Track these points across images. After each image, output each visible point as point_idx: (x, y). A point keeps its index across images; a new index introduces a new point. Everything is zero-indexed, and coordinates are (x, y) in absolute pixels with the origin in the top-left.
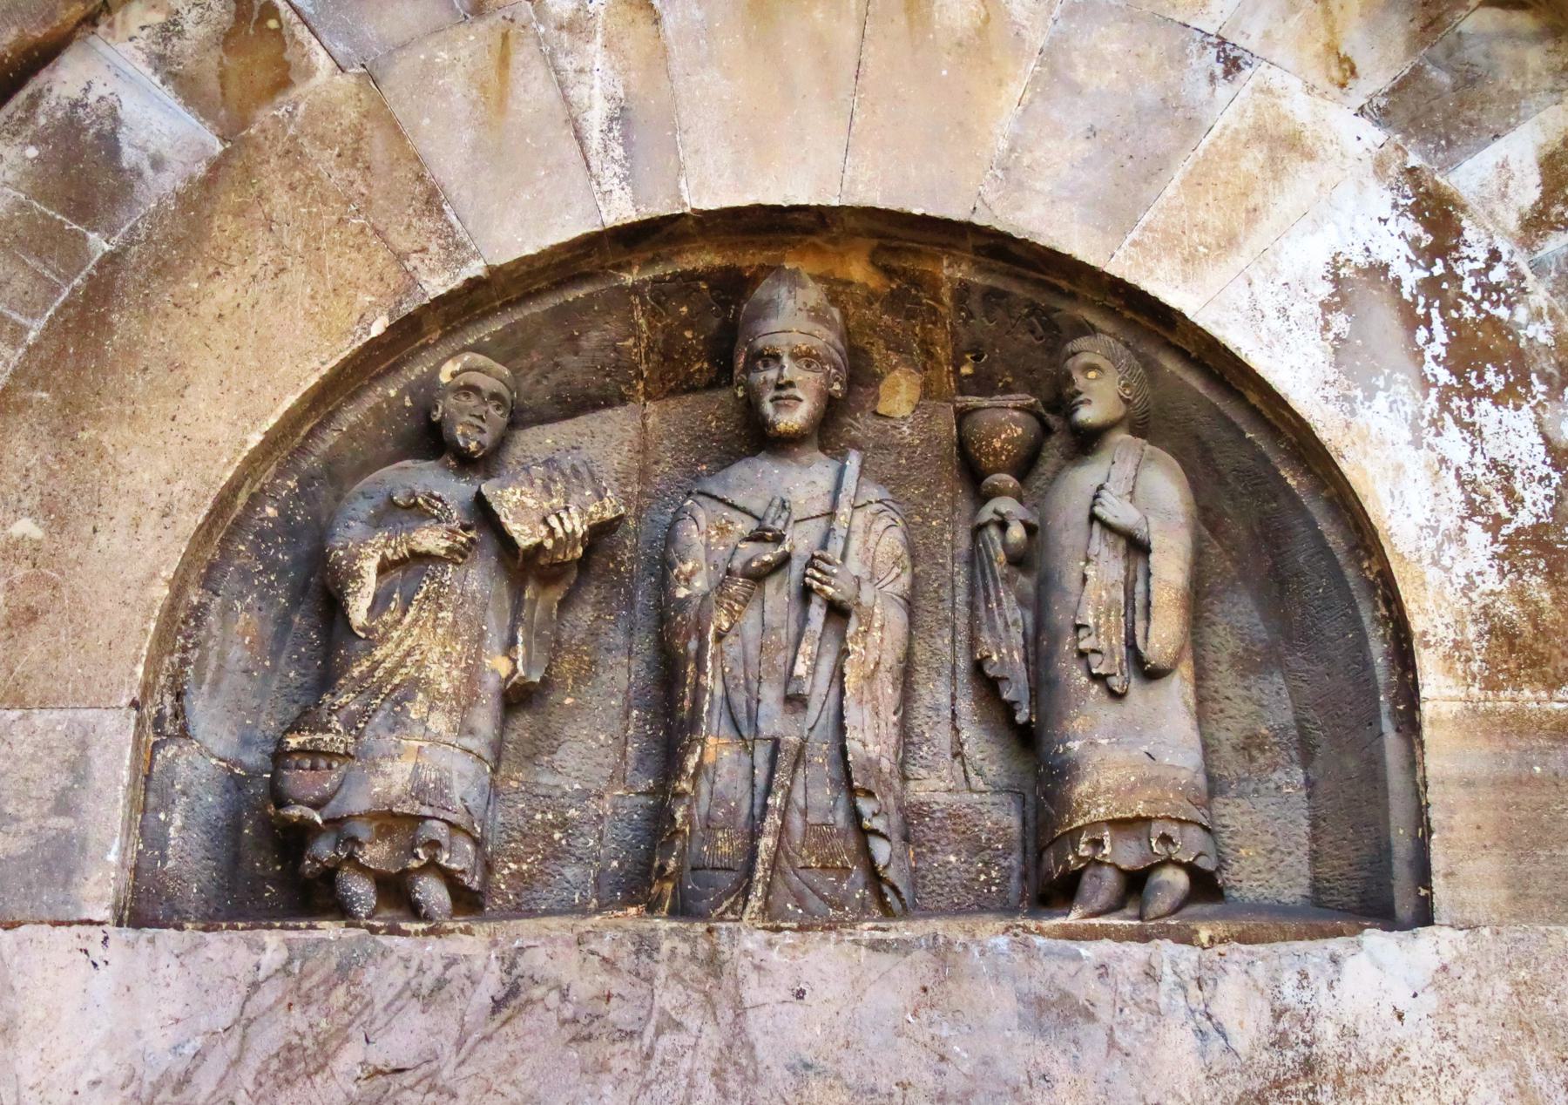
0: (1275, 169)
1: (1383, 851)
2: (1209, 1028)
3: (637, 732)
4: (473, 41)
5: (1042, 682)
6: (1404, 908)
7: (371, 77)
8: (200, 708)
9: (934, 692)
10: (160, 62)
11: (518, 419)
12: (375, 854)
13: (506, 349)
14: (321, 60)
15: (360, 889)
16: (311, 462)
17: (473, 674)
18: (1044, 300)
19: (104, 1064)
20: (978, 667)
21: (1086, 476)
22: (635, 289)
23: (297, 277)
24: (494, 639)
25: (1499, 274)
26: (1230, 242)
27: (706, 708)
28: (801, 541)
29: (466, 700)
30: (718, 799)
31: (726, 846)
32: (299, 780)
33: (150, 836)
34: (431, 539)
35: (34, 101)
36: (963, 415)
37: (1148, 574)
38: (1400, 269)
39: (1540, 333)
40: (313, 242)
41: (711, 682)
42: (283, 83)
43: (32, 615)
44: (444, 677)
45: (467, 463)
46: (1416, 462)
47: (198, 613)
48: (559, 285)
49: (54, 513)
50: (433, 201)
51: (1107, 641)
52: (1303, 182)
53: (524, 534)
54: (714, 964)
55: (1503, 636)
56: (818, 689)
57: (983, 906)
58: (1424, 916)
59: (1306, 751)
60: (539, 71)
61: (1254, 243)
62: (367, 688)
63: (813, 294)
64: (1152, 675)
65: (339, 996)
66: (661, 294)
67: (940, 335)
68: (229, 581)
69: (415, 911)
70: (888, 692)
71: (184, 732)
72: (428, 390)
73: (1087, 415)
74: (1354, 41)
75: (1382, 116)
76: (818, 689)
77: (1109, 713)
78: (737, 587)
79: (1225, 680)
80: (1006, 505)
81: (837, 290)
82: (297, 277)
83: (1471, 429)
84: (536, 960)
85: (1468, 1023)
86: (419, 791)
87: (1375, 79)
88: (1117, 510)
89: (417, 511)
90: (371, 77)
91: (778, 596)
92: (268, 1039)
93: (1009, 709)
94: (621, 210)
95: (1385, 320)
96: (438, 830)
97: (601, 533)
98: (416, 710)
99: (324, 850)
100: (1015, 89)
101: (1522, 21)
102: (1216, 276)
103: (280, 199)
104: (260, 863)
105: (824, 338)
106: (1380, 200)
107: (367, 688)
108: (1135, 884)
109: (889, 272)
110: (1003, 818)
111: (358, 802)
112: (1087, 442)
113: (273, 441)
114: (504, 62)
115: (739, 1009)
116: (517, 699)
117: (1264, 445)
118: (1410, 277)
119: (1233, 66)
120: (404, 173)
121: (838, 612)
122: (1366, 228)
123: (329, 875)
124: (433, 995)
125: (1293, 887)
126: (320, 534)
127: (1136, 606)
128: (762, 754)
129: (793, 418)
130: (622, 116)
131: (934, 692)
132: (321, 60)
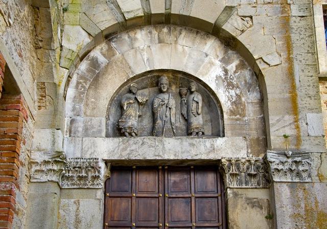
1: (219, 131)
2: (205, 146)
3: (150, 120)
6: (221, 136)
7: (123, 55)
8: (110, 117)
10: (101, 53)
14: (117, 53)
15: (127, 134)
16: (119, 94)
17: (136, 114)
18: (189, 79)
19: (106, 150)
20: (182, 114)
21: (192, 96)
22: (149, 77)
23: (117, 75)
24: (138, 111)
25: (231, 77)
26: (207, 74)
27: (181, 120)
28: (166, 102)
30: (160, 126)
31: (161, 130)
32: (120, 124)
33: (107, 129)
34: (131, 101)
35: (89, 56)
36: (180, 90)
37: (62, 31)
38: (222, 76)
39: (235, 83)
40: (118, 72)
41: (158, 115)
42: (114, 55)
43: (95, 108)
44: (133, 114)
45: (134, 94)
46: (224, 95)
47: (110, 108)
48: (142, 76)
50: (130, 68)
51: (195, 111)
52: (214, 68)
54: (161, 141)
55: (231, 111)
56: (168, 115)
57: (182, 136)
58: (224, 136)
59: (211, 121)
60: (140, 54)
61: (209, 73)
62: (126, 116)
63: (166, 78)
64: (199, 114)
65: (127, 144)
66: (152, 78)
67: (178, 82)
68: (112, 105)
69: (132, 136)
71: (109, 120)
72: (130, 87)
73: (192, 90)
74: (218, 53)
75: (221, 61)
76: (168, 115)
77: (195, 118)
78: (161, 106)
80: (184, 99)
81: (168, 77)
82: (117, 75)
83: (229, 92)
84: (145, 140)
85: (228, 145)
86: (132, 125)
87: (220, 57)
88: (195, 99)
89: (130, 99)
90: (123, 55)
91: (164, 107)
93: (185, 118)
94: (148, 69)
95: (221, 81)
96: (134, 128)
97: (147, 100)
98: (131, 117)
99: (123, 130)
100: (186, 58)
101: (234, 52)
102: (205, 77)
103: (115, 67)
104: (117, 132)
106: (221, 70)
107: (126, 116)
108: (197, 133)
109: (173, 76)
110: (184, 127)
111: (126, 126)
112: (192, 93)
113: (116, 91)
114: (136, 54)
115: (164, 145)
116: (140, 116)
117: (209, 93)
118: (223, 77)
119: (207, 55)
120: (127, 65)
121: (170, 108)
122: (220, 73)
123: (124, 133)
124: (135, 144)
125: (210, 134)
127: (197, 108)
128: (163, 121)
129: (165, 90)
130: (148, 60)
131: (178, 116)
132: (117, 53)
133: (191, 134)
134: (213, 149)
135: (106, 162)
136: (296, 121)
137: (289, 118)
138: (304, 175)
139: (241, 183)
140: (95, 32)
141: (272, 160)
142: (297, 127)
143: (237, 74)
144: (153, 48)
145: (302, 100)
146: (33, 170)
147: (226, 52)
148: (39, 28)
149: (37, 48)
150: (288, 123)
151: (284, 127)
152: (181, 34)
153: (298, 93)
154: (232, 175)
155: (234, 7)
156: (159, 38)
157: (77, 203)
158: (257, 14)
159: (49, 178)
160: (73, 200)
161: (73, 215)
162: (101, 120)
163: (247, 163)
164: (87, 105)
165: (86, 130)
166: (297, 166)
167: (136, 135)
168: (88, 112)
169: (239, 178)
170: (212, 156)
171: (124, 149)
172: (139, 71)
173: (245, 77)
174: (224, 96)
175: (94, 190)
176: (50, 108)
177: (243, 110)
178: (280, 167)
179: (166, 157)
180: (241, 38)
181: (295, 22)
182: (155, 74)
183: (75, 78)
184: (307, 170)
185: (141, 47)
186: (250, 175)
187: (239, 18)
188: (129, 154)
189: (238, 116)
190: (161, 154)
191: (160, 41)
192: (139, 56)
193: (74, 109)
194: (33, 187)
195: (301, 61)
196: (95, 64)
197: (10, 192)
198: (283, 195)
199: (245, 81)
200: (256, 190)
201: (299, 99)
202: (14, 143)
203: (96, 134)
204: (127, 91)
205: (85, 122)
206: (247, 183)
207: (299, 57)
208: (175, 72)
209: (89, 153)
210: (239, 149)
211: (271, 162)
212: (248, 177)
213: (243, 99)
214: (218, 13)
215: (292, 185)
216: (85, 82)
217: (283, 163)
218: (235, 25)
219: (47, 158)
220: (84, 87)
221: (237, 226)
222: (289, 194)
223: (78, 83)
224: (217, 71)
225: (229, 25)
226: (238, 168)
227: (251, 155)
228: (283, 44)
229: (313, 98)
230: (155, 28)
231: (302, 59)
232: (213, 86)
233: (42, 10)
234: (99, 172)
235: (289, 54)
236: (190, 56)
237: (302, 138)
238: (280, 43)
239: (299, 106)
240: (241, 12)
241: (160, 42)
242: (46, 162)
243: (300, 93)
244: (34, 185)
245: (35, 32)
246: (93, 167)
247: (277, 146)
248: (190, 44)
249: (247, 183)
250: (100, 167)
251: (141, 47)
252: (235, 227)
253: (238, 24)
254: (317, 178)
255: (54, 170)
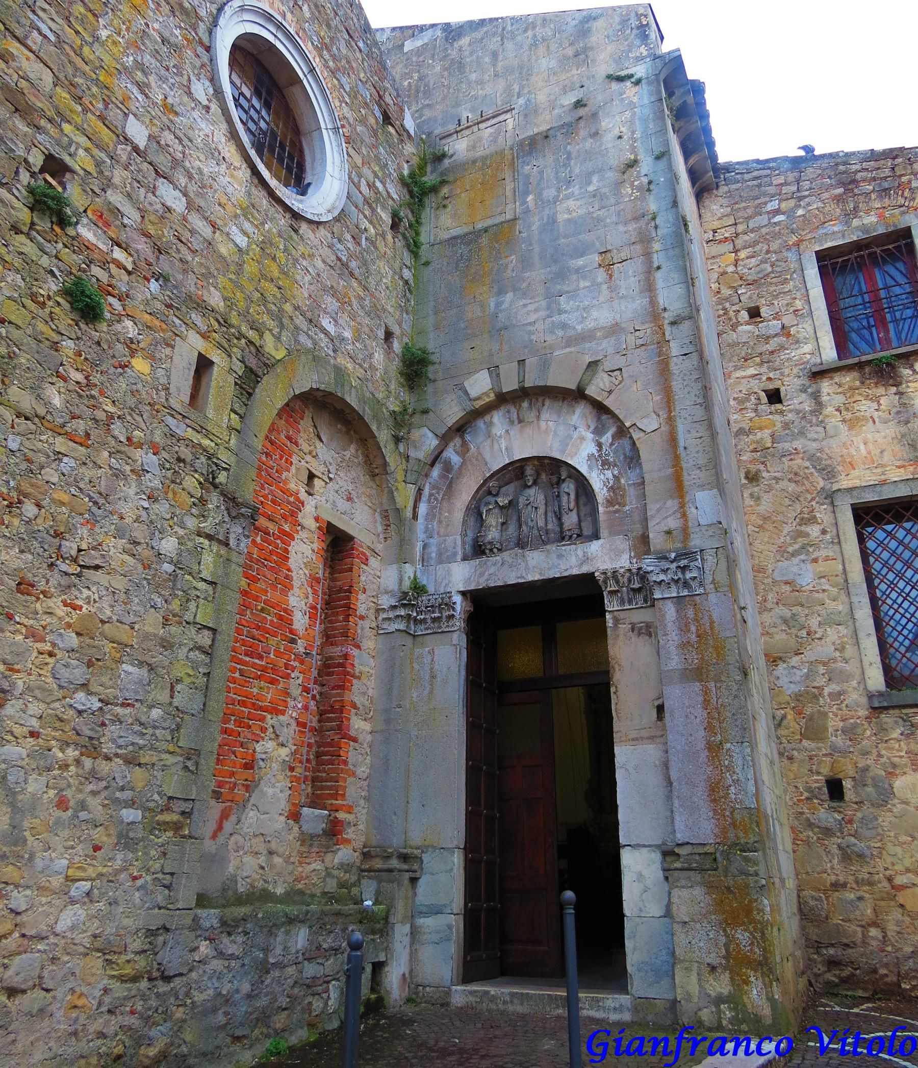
0: (581, 443)
2: (577, 555)
4: (489, 441)
5: (560, 513)
9: (549, 514)
11: (500, 488)
12: (488, 547)
13: (497, 480)
15: (487, 551)
23: (472, 477)
26: (576, 454)
29: (497, 526)
32: (480, 539)
34: (491, 507)
44: (494, 524)
46: (598, 480)
49: (449, 512)
52: (585, 443)
53: (501, 504)
54: (524, 556)
63: (531, 467)
66: (514, 470)
70: (543, 516)
75: (593, 433)
79: (582, 507)
87: (592, 428)
92: (478, 572)
94: (507, 461)
95: (594, 461)
102: (575, 458)
105: (533, 472)
106: (593, 445)
108: (571, 537)
116: (503, 524)
121: (536, 508)
124: (495, 564)
126: (479, 507)
127: (569, 502)
130: (506, 449)
133: (563, 539)
134: (586, 559)
135: (463, 593)
136: (682, 506)
137: (672, 504)
138: (694, 584)
139: (622, 602)
140: (442, 430)
141: (650, 569)
142: (684, 515)
143: (613, 447)
144: (512, 433)
145: (689, 475)
146: (380, 618)
147: (599, 419)
148: (371, 457)
149: (373, 476)
150: (671, 511)
151: (667, 517)
152: (543, 405)
153: (684, 465)
154: (611, 592)
155: (599, 361)
156: (518, 418)
157: (432, 652)
158: (628, 363)
159: (397, 626)
160: (427, 649)
161: (427, 668)
162: (456, 541)
163: (628, 574)
164: (440, 522)
165: (440, 554)
166: (683, 573)
167: (499, 550)
168: (442, 530)
169: (619, 595)
170: (585, 569)
171: (482, 574)
172: (496, 467)
173: (624, 449)
174: (598, 481)
175: (449, 634)
176: (396, 538)
177: (623, 496)
178: (662, 577)
179: (530, 578)
180: (606, 403)
181: (676, 364)
182: (518, 465)
183: (426, 491)
184: (695, 578)
185: (498, 434)
186: (633, 590)
187: (605, 375)
188: (487, 580)
189: (617, 507)
190: (524, 574)
191: (520, 421)
192: (496, 446)
193: (427, 530)
194: (380, 638)
195: (685, 419)
196: (448, 467)
197: (346, 656)
198: (667, 616)
199: (625, 455)
200: (642, 610)
201: (685, 477)
202: (348, 598)
203: (451, 559)
204: (485, 492)
205: (439, 545)
206: (630, 602)
207: (684, 414)
208: (539, 458)
209: (443, 584)
210: (618, 554)
211: (648, 573)
212: (631, 593)
213: (623, 481)
214: (580, 374)
215: (679, 600)
216: (438, 493)
217: (665, 571)
218: (601, 385)
219: (393, 602)
220: (436, 499)
221: (619, 665)
222: (674, 614)
223: (431, 495)
224: (590, 448)
225: (593, 387)
226: (617, 582)
227: (635, 560)
228: (661, 399)
229: (703, 469)
230: (514, 403)
231: (687, 416)
232: (584, 469)
233: (370, 441)
234: (454, 609)
235: (670, 411)
236: (555, 434)
237: (691, 530)
238: (658, 398)
239: (686, 483)
240: (608, 365)
241: (520, 421)
242: (394, 607)
243: (687, 464)
244: (382, 637)
245: (368, 461)
246: (446, 604)
247: (658, 547)
248: (554, 417)
249: (630, 602)
250: (454, 603)
251: (498, 434)
252: (616, 666)
253: (604, 383)
254: (712, 586)
255: (402, 616)
